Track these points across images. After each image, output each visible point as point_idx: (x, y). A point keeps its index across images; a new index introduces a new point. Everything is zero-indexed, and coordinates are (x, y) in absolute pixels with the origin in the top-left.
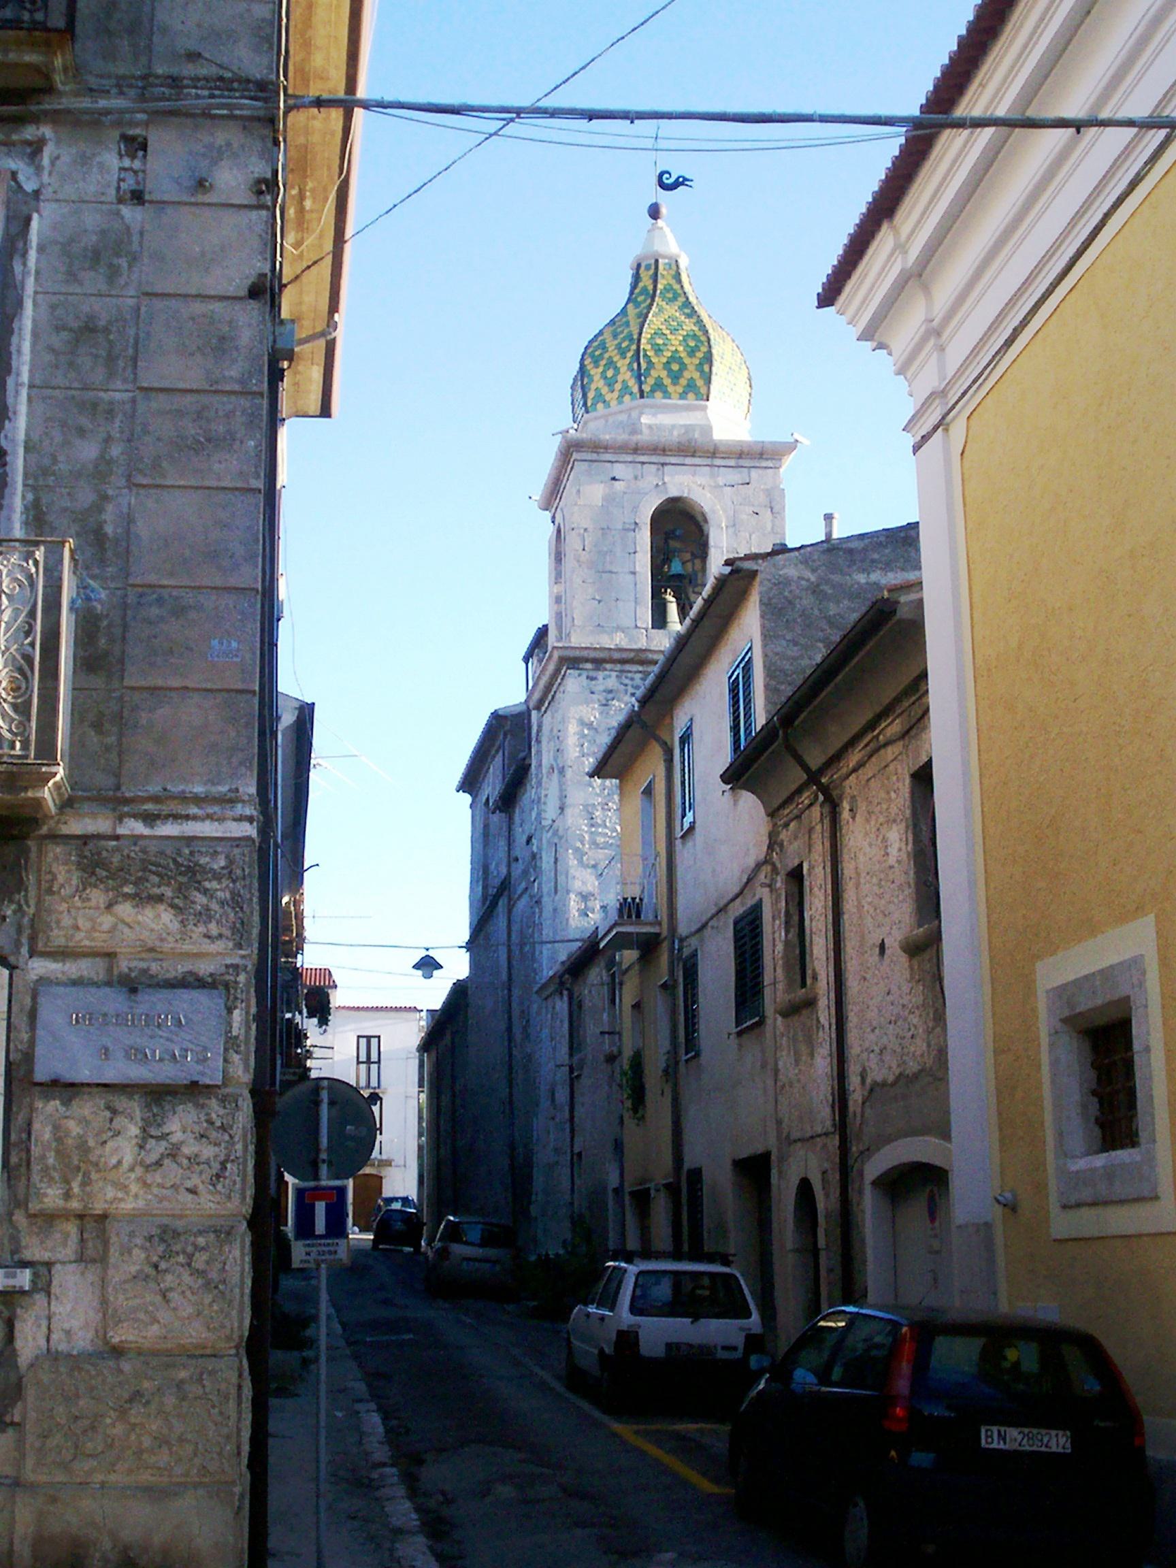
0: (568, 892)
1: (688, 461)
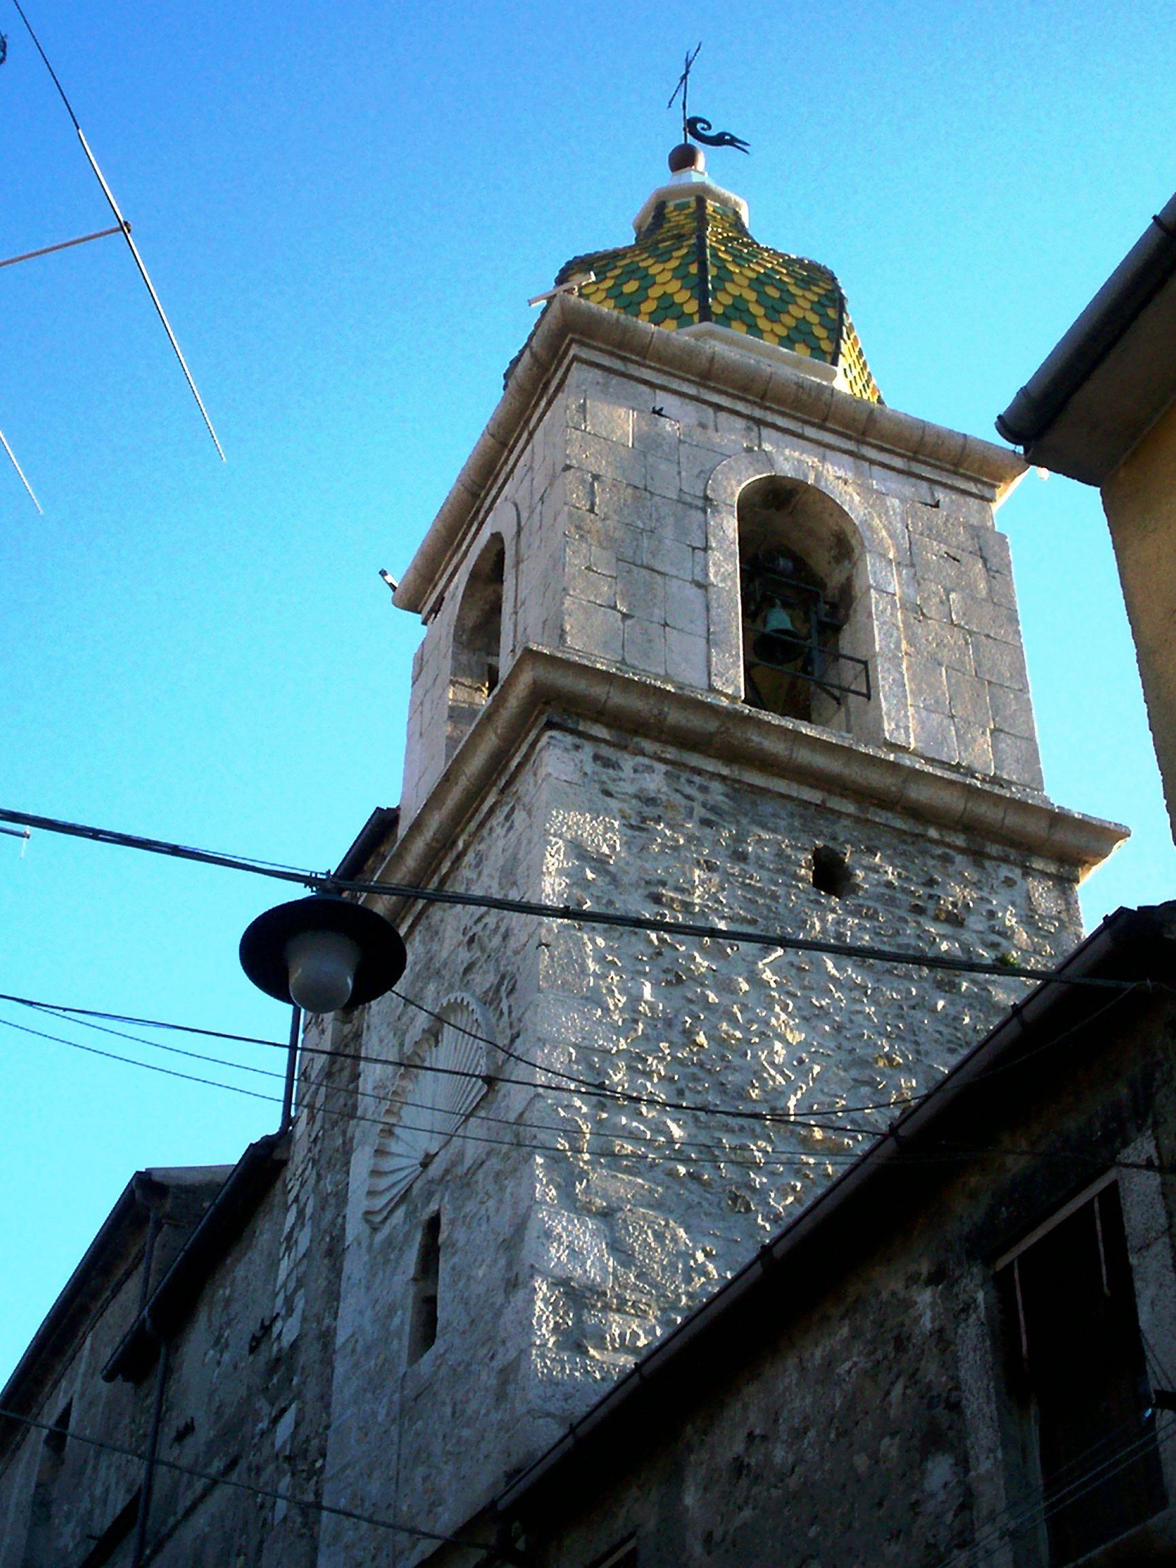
0: (533, 1271)
1: (810, 432)
